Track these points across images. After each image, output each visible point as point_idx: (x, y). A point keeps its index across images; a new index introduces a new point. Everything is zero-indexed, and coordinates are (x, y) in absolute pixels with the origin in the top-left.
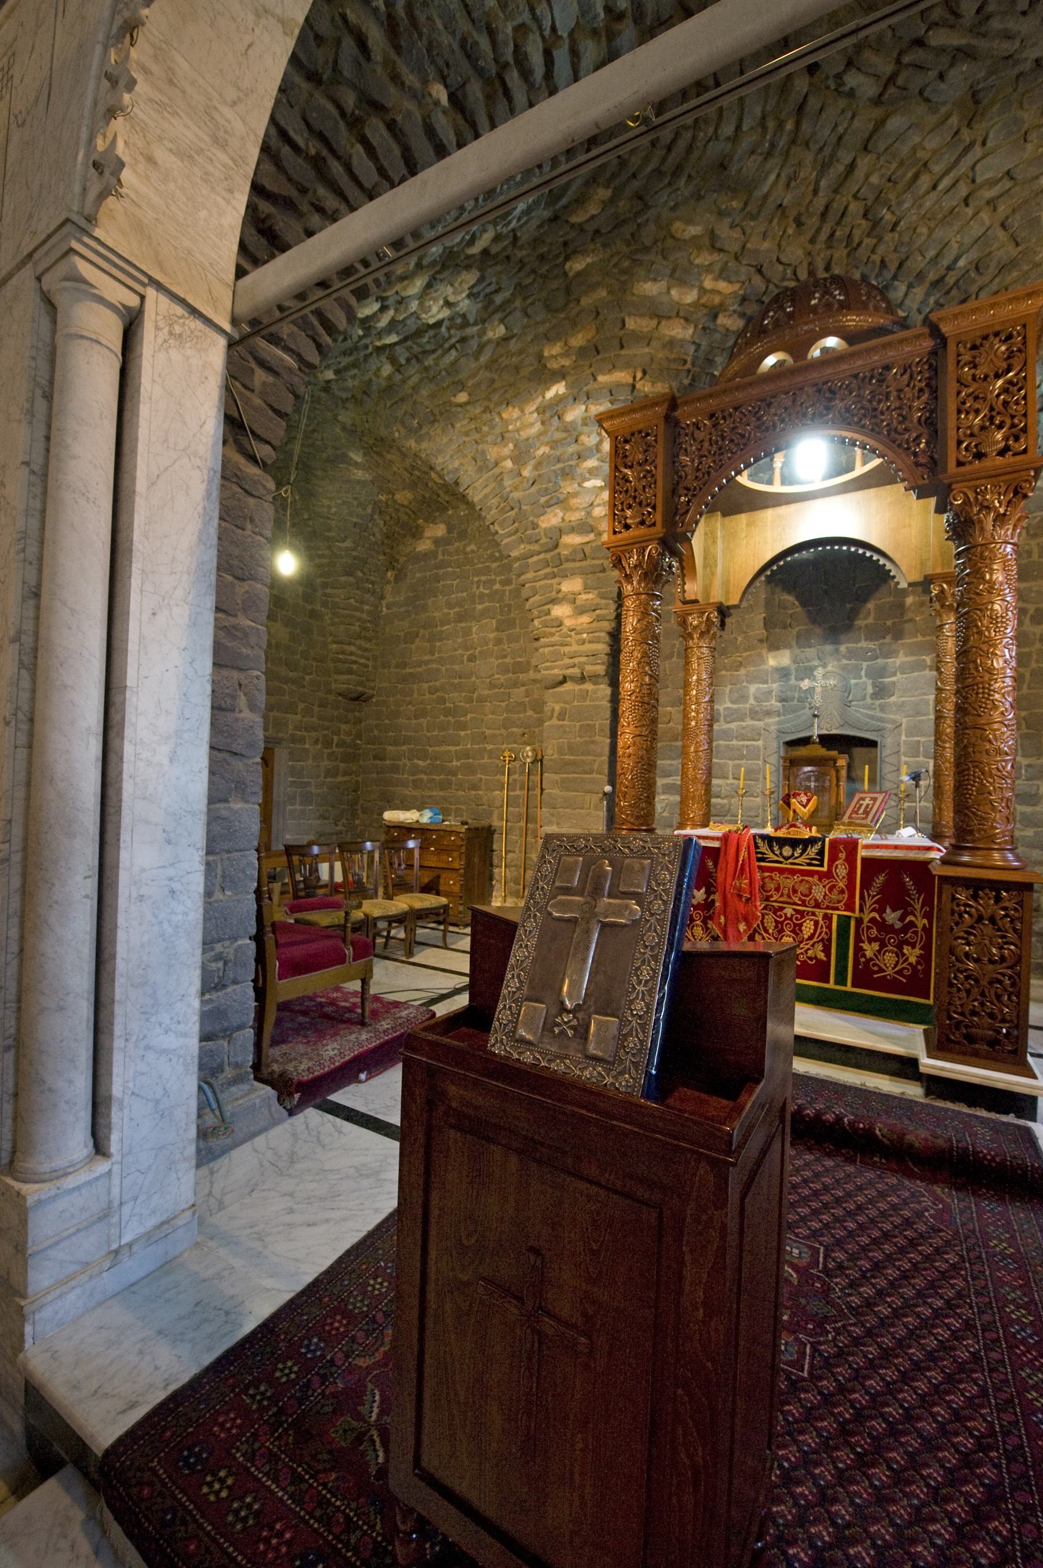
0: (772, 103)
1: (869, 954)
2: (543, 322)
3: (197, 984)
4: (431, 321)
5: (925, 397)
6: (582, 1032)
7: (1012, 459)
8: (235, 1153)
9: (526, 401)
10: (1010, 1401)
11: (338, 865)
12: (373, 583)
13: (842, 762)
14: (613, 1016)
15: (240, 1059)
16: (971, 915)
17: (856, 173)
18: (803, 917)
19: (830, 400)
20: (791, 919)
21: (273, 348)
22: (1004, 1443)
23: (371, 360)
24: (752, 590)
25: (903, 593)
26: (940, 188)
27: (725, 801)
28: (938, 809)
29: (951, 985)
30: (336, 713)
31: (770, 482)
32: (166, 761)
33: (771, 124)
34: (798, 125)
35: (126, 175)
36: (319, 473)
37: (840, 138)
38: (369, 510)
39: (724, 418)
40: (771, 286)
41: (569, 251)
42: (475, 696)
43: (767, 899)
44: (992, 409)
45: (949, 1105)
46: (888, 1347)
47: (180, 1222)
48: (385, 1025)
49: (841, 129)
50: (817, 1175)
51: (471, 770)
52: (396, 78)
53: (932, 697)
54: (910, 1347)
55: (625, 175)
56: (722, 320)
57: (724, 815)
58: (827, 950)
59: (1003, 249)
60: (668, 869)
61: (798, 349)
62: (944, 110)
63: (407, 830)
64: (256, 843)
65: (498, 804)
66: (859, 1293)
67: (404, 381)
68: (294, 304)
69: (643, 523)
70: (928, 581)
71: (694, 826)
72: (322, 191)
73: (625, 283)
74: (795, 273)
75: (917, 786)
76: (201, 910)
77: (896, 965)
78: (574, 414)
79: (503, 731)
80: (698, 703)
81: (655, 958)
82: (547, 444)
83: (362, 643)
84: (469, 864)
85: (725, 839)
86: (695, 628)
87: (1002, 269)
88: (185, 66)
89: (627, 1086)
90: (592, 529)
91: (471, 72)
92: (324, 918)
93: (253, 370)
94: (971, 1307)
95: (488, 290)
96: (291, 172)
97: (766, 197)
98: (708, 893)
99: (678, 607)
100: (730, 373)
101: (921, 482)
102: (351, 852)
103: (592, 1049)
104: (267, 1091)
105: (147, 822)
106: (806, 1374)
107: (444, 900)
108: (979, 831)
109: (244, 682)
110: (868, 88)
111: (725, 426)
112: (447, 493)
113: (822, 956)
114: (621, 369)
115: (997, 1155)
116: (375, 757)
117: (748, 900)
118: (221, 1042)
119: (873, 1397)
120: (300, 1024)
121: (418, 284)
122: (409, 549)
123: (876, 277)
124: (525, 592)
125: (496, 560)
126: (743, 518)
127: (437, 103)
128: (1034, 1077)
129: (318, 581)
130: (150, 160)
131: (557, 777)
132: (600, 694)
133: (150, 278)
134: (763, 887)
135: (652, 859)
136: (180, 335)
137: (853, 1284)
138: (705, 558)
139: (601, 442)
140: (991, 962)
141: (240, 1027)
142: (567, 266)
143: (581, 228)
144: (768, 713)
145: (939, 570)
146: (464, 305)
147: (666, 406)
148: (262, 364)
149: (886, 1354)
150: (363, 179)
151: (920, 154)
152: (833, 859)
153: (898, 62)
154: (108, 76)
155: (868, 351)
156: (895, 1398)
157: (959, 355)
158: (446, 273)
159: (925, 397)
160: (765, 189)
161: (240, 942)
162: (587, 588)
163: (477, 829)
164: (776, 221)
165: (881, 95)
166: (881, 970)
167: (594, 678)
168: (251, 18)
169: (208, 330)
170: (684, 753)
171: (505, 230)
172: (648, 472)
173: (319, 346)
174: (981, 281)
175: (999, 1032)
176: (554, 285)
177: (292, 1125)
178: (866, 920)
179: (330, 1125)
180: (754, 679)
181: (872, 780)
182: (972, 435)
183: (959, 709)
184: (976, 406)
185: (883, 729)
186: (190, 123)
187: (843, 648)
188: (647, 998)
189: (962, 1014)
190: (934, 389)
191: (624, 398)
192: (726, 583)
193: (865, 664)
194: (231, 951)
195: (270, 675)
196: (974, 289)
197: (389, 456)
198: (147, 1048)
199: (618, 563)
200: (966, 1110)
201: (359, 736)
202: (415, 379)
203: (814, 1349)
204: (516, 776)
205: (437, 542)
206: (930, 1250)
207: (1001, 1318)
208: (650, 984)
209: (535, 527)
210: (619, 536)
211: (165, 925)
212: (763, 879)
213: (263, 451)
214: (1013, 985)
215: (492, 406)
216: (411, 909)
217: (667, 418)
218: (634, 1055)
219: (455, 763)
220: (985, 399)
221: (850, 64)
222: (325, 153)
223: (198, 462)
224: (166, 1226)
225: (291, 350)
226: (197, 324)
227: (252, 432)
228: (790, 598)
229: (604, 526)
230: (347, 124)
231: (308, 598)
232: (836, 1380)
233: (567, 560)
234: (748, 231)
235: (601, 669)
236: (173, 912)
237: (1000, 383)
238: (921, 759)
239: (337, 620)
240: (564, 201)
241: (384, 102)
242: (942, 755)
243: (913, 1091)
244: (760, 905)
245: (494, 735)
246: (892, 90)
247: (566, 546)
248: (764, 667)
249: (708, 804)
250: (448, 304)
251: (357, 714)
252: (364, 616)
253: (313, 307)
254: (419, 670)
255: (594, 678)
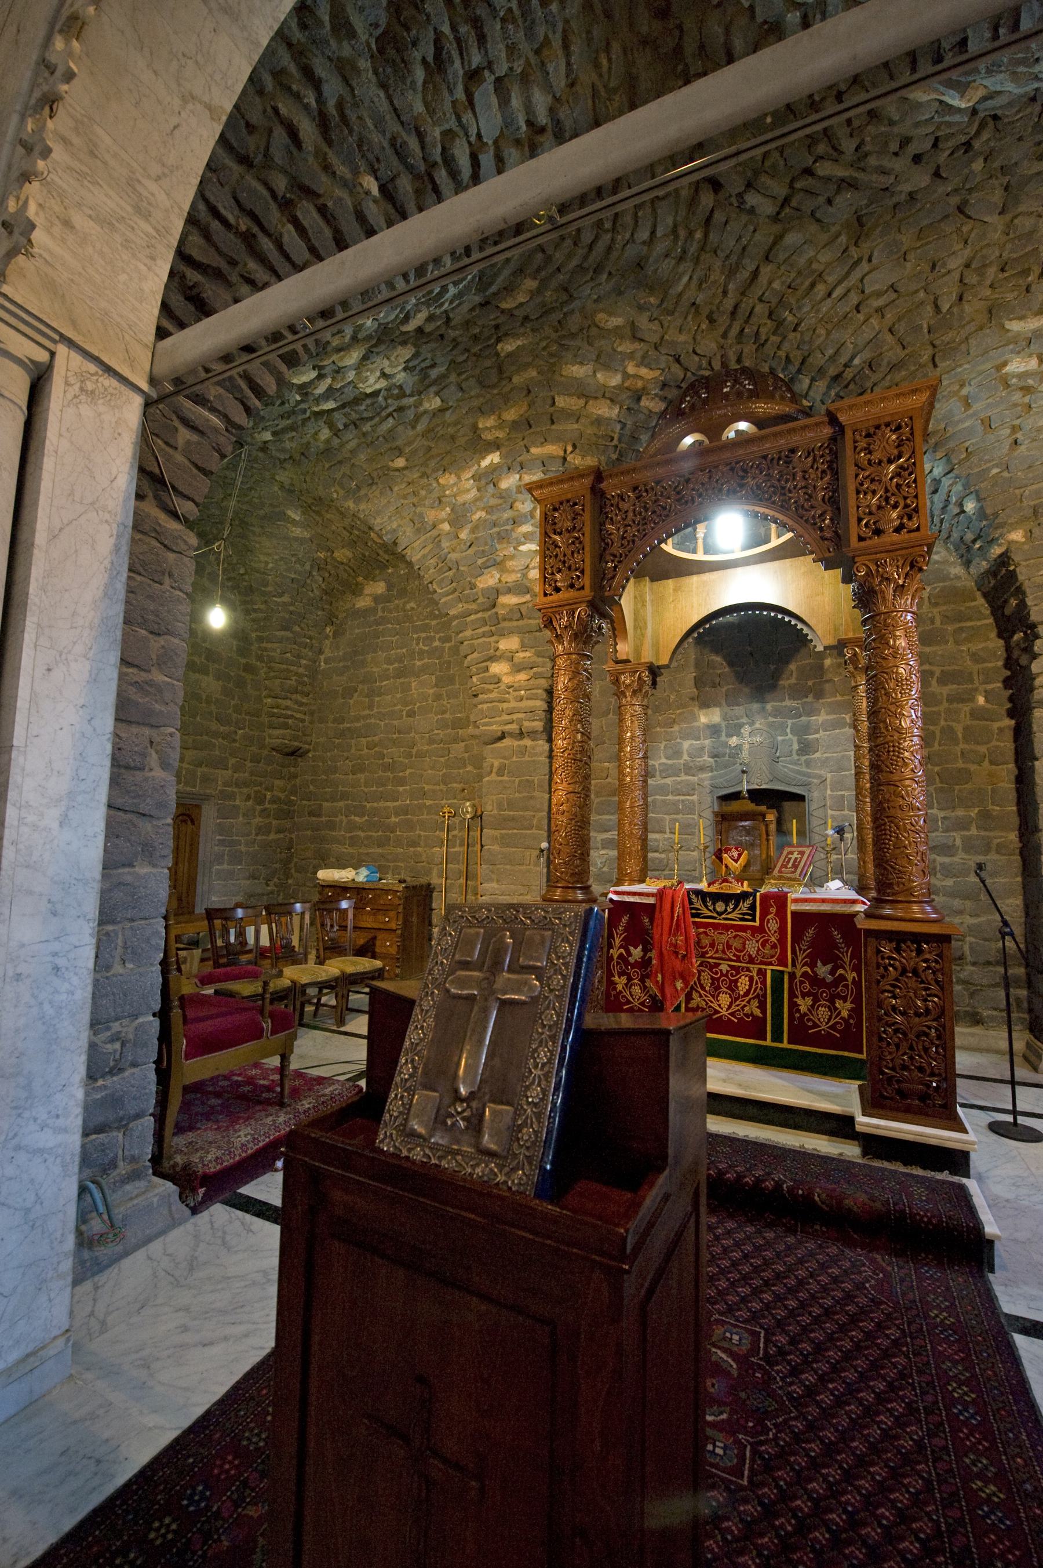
0: (682, 212)
1: (803, 1009)
2: (478, 396)
3: (82, 1070)
4: (369, 391)
5: (827, 478)
6: (476, 1124)
7: (907, 536)
8: (126, 1263)
9: (463, 469)
10: (954, 1494)
11: (264, 929)
12: (311, 638)
13: (771, 817)
14: (508, 1104)
15: (136, 1152)
16: (895, 969)
17: (760, 279)
18: (738, 973)
19: (743, 478)
20: (726, 975)
21: (200, 410)
22: (951, 1544)
23: (309, 424)
24: (681, 650)
25: (821, 656)
26: (834, 295)
27: (663, 856)
28: (862, 860)
29: (881, 1039)
30: (269, 769)
31: (694, 551)
32: (55, 825)
33: (682, 233)
34: (706, 235)
35: (37, 236)
36: (257, 530)
37: (744, 249)
38: (308, 567)
39: (646, 491)
40: (689, 374)
41: (500, 333)
42: (414, 751)
43: (703, 955)
44: (887, 491)
45: (886, 1165)
46: (831, 1442)
47: (51, 1352)
48: (306, 1104)
49: (744, 241)
50: (758, 1249)
51: (410, 826)
52: (327, 168)
53: (852, 753)
54: (853, 1440)
55: (550, 269)
56: (645, 402)
57: (662, 869)
58: (762, 1006)
59: (893, 353)
60: (568, 941)
61: (714, 431)
62: (834, 229)
63: (342, 889)
64: (163, 911)
65: (437, 860)
66: (801, 1382)
67: (342, 445)
68: (218, 367)
69: (572, 586)
70: (841, 645)
71: (632, 882)
72: (252, 265)
73: (554, 364)
74: (710, 364)
75: (841, 840)
76: (90, 989)
77: (829, 1020)
78: (509, 482)
79: (442, 787)
80: (632, 759)
81: (553, 1038)
82: (483, 509)
83: (299, 697)
84: (406, 923)
85: (660, 894)
86: (628, 686)
87: (893, 367)
88: (108, 140)
89: (520, 1184)
90: (528, 591)
91: (401, 168)
92: (246, 988)
93: (176, 429)
94: (914, 1389)
95: (423, 365)
96: (221, 245)
97: (680, 295)
98: (645, 950)
99: (611, 666)
100: (652, 450)
101: (827, 555)
102: (280, 914)
103: (487, 1140)
104: (169, 1187)
105: (30, 893)
106: (746, 1483)
107: (378, 964)
108: (898, 883)
109: (157, 739)
110: (767, 208)
111: (647, 498)
112: (386, 552)
113: (758, 1012)
114: (553, 443)
115: (933, 1216)
116: (311, 814)
117: (684, 956)
118: (115, 1134)
119: (816, 1502)
120: (212, 1107)
121: (353, 357)
122: (348, 606)
123: (783, 370)
124: (464, 649)
125: (436, 617)
126: (670, 583)
127: (368, 193)
128: (965, 1131)
129: (254, 635)
130: (67, 224)
131: (497, 833)
132: (538, 750)
133: (61, 335)
134: (698, 942)
135: (553, 930)
136: (93, 392)
137: (795, 1372)
138: (635, 620)
139: (535, 508)
140: (918, 1015)
141: (138, 1116)
142: (499, 347)
143: (510, 313)
144: (702, 769)
145: (851, 635)
146: (401, 377)
147: (592, 478)
148: (186, 423)
149: (830, 1450)
150: (294, 257)
151: (814, 266)
152: (764, 913)
153: (791, 186)
154: (23, 143)
155: (775, 435)
156: (879, 1457)
157: (855, 442)
158: (383, 347)
159: (827, 478)
160: (680, 288)
161: (141, 1020)
162: (524, 647)
163: (414, 887)
164: (690, 317)
165: (778, 213)
166: (816, 1025)
167: (532, 734)
168: (177, 102)
169: (123, 388)
170: (620, 807)
171: (438, 312)
172: (577, 538)
173: (248, 410)
174: (875, 378)
175: (929, 1086)
176: (488, 363)
177: (195, 1225)
178: (798, 974)
179: (237, 1223)
180: (686, 736)
181: (801, 833)
182: (870, 513)
183: (873, 766)
184: (873, 487)
185: (809, 784)
186: (112, 193)
187: (769, 707)
188: (543, 1083)
189: (893, 1069)
190: (834, 469)
191: (556, 469)
192: (656, 645)
193: (790, 722)
194: (131, 1029)
195: (184, 729)
196: (869, 384)
197: (328, 516)
198: (18, 1148)
199: (549, 624)
200: (902, 1169)
201: (293, 792)
202: (352, 444)
203: (754, 1452)
204: (455, 832)
205: (376, 599)
206: (871, 1326)
207: (943, 1398)
208: (546, 1069)
209: (473, 586)
210: (549, 598)
211: (46, 1007)
212: (698, 934)
213: (186, 508)
214: (939, 1037)
215: (429, 472)
216: (343, 973)
217: (594, 490)
218: (528, 1148)
219: (393, 819)
220: (880, 481)
221: (749, 185)
222: (255, 230)
223: (107, 516)
224: (32, 1359)
225: (219, 411)
226: (111, 382)
227: (173, 487)
228: (718, 659)
229: (537, 588)
230: (280, 206)
231: (243, 652)
232: (777, 1486)
233: (505, 620)
234: (666, 324)
235: (539, 725)
236: (56, 991)
237: (892, 467)
238: (846, 812)
239: (272, 674)
240: (493, 289)
241: (314, 187)
242: (863, 810)
243: (851, 1151)
244: (696, 962)
245: (434, 791)
246: (787, 210)
247: (504, 606)
248: (696, 724)
249: (645, 858)
250: (384, 375)
251: (292, 769)
252: (301, 670)
253: (240, 369)
254: (358, 725)
255: (532, 734)
